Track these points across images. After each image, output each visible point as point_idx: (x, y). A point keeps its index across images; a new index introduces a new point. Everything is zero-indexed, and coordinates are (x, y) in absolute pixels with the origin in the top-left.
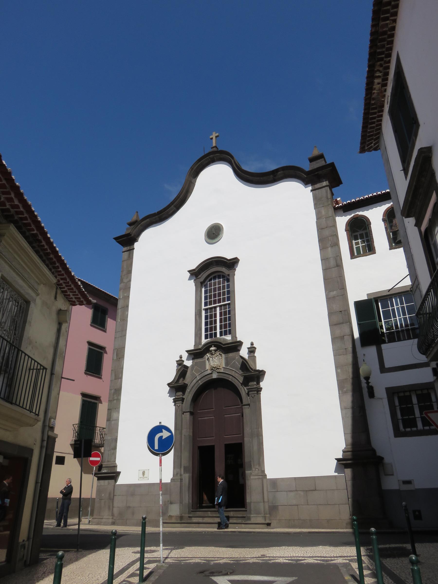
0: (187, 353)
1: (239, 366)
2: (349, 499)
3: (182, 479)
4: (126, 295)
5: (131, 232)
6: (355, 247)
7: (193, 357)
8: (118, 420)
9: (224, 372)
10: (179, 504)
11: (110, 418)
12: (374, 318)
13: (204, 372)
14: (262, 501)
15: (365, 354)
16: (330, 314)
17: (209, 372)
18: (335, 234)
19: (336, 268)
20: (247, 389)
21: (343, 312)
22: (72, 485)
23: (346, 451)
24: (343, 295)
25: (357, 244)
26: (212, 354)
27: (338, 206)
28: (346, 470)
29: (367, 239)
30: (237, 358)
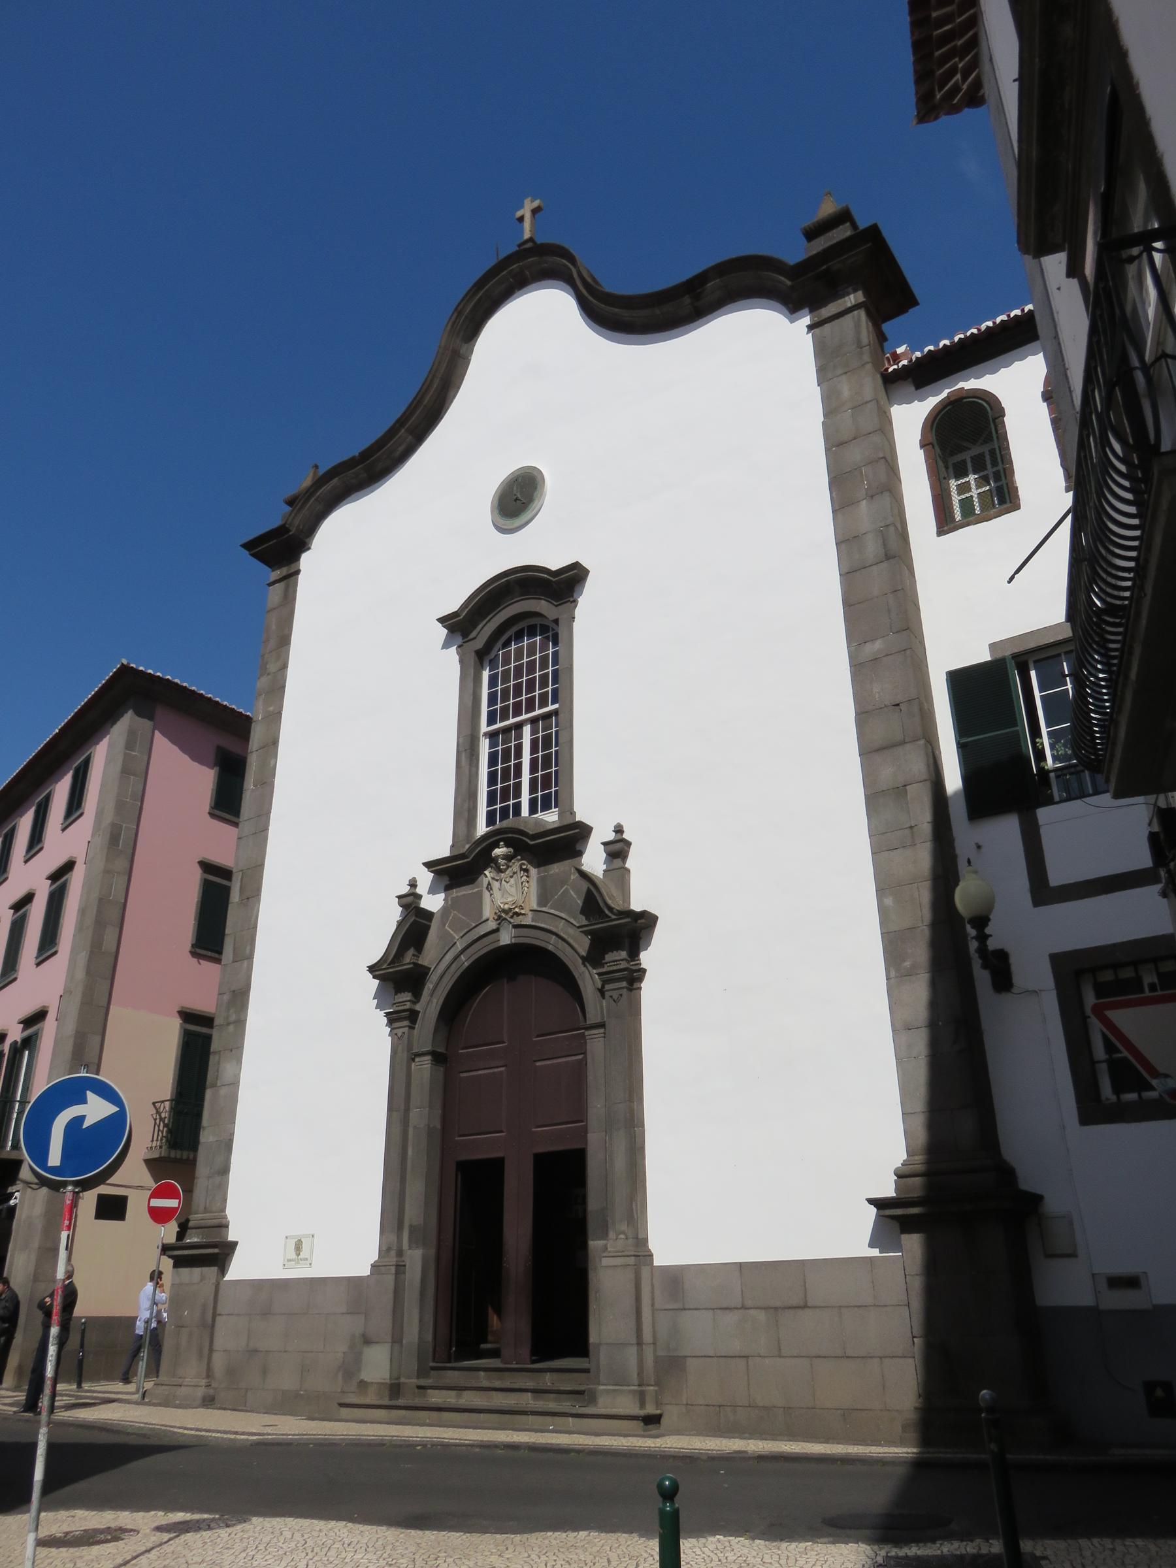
0: (427, 869)
1: (580, 902)
2: (915, 1339)
3: (405, 1266)
4: (271, 709)
5: (288, 522)
6: (956, 499)
7: (448, 883)
9: (533, 924)
10: (390, 1344)
11: (217, 1079)
12: (1012, 719)
14: (634, 1341)
15: (980, 844)
16: (863, 716)
17: (492, 925)
18: (881, 456)
19: (885, 565)
20: (599, 974)
21: (902, 706)
22: (75, 1282)
23: (907, 1173)
24: (905, 650)
25: (964, 488)
26: (500, 871)
27: (896, 367)
28: (905, 1238)
29: (995, 469)
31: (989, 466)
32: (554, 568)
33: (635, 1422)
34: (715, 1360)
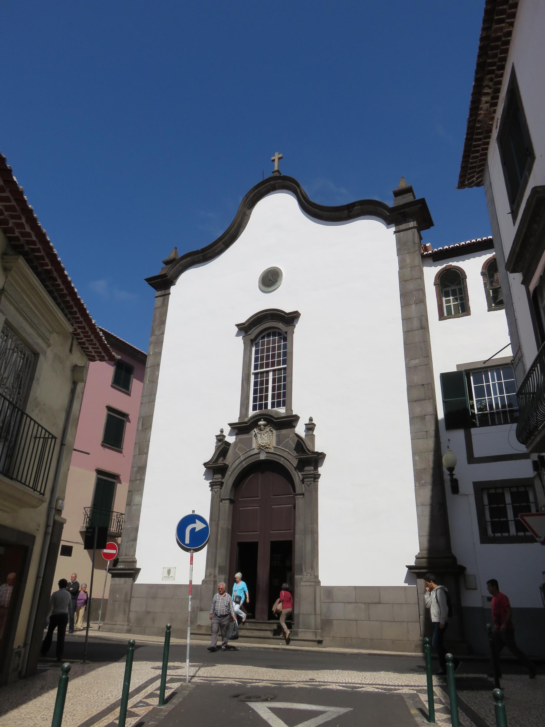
1: (294, 446)
4: (157, 350)
6: (445, 305)
7: (237, 432)
11: (131, 502)
14: (313, 613)
16: (410, 388)
17: (256, 451)
18: (421, 288)
19: (421, 331)
21: (425, 386)
25: (448, 302)
26: (261, 430)
27: (427, 253)
28: (418, 580)
31: (458, 294)
32: (287, 312)
33: (314, 642)
34: (344, 621)
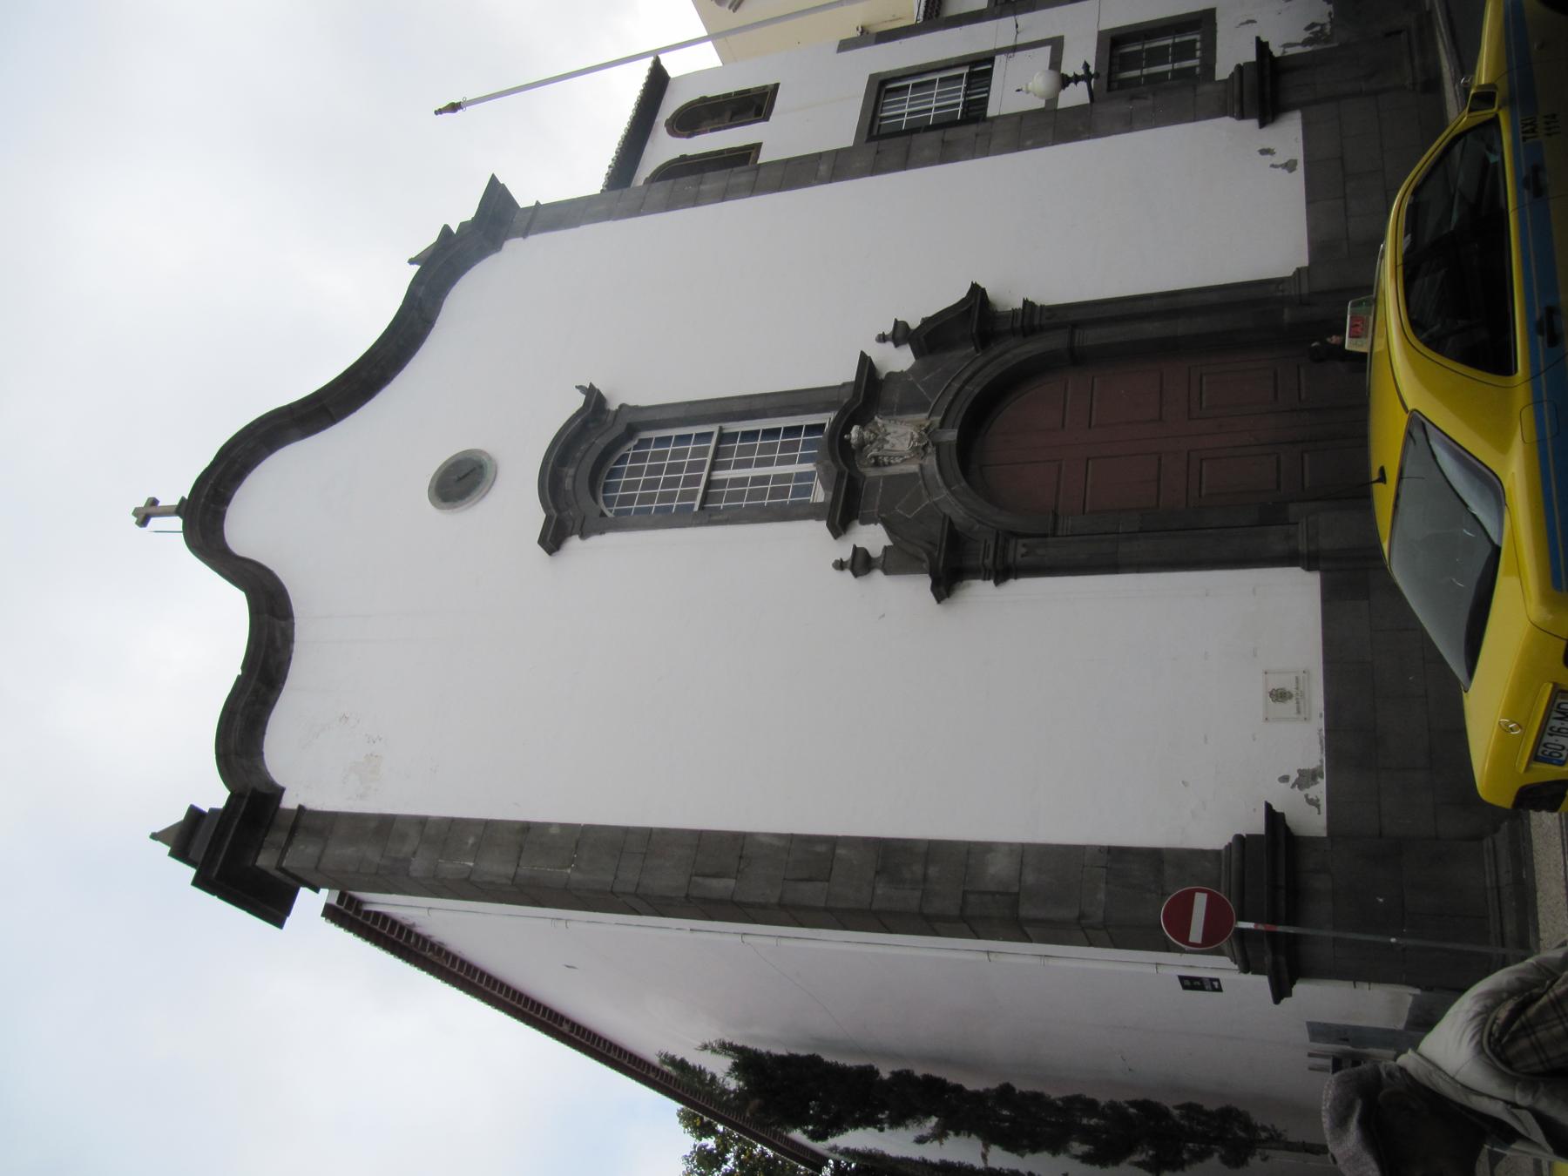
4: (471, 841)
8: (1023, 851)
13: (924, 480)
30: (911, 379)
